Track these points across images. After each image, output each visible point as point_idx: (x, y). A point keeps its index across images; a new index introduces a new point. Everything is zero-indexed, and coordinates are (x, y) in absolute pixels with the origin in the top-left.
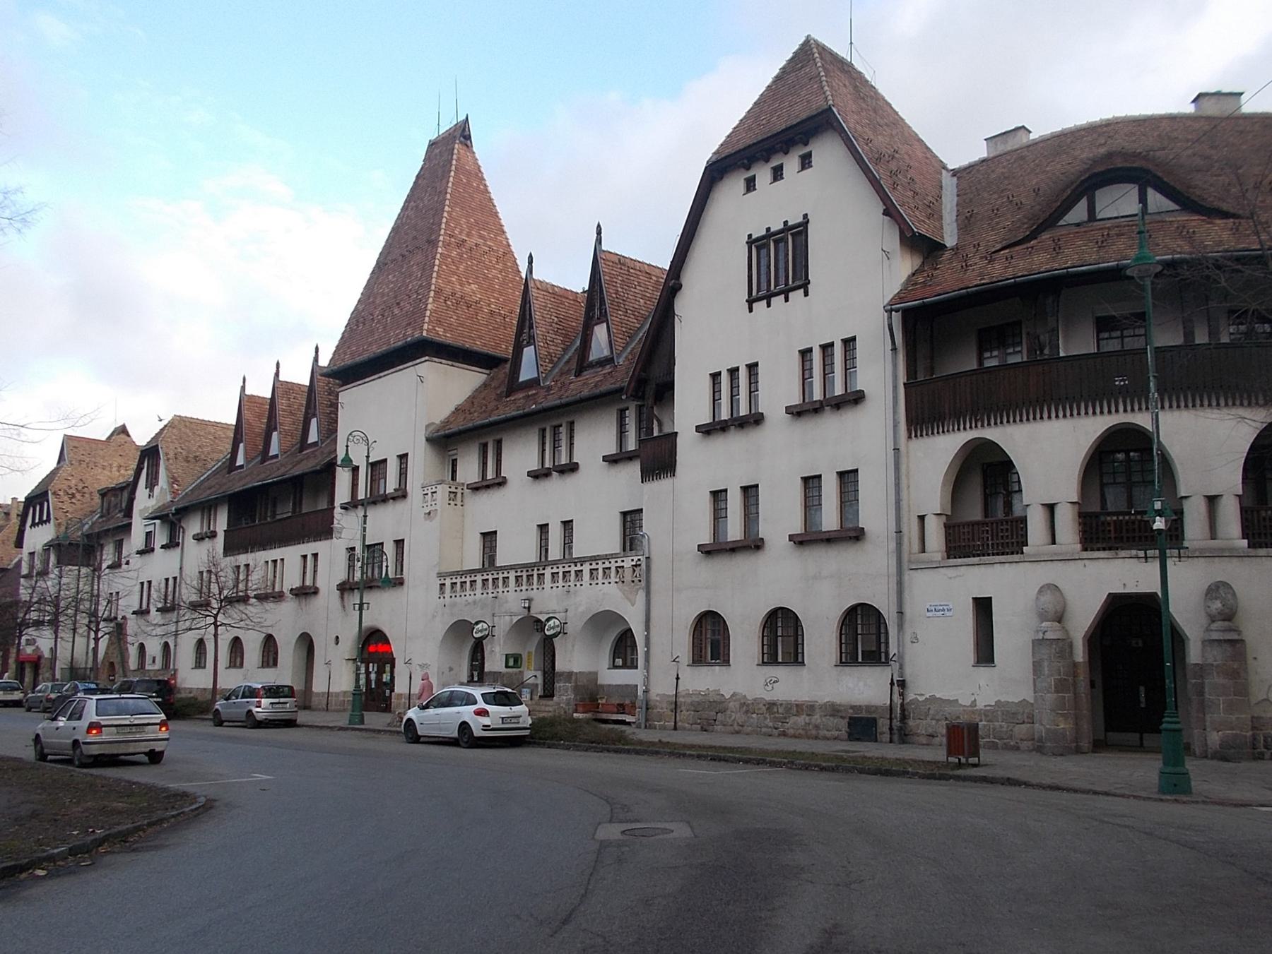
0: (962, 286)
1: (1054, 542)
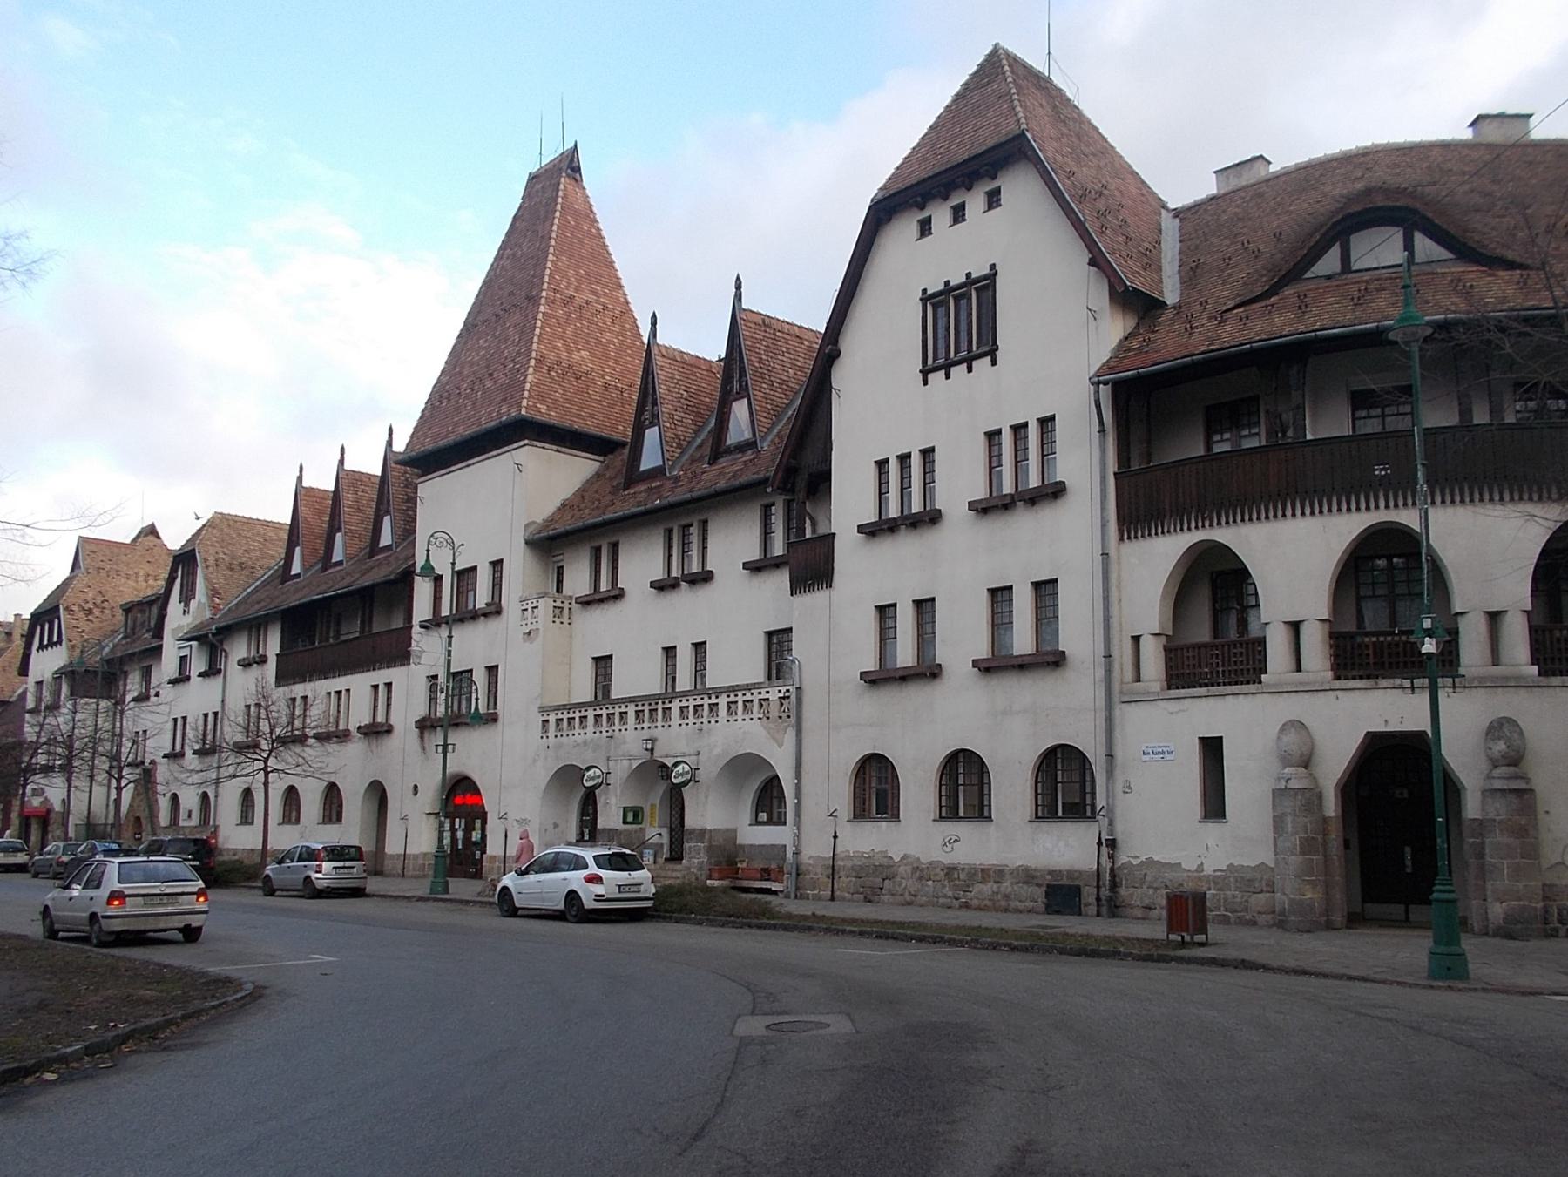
0: (1185, 352)
1: (1299, 669)
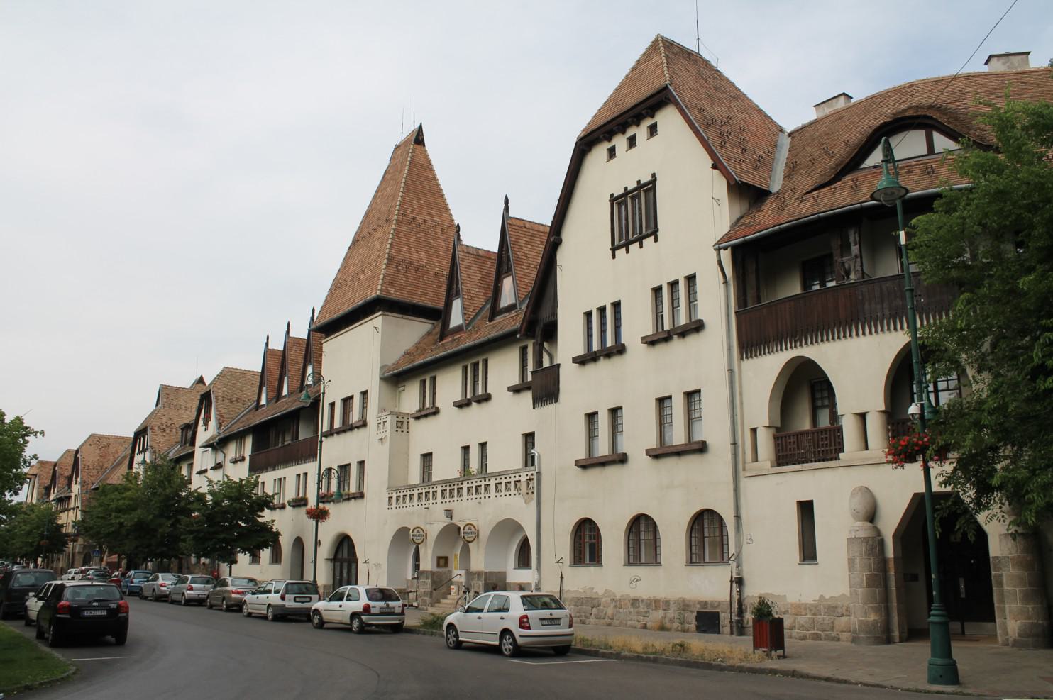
0: (776, 223)
1: (867, 448)
